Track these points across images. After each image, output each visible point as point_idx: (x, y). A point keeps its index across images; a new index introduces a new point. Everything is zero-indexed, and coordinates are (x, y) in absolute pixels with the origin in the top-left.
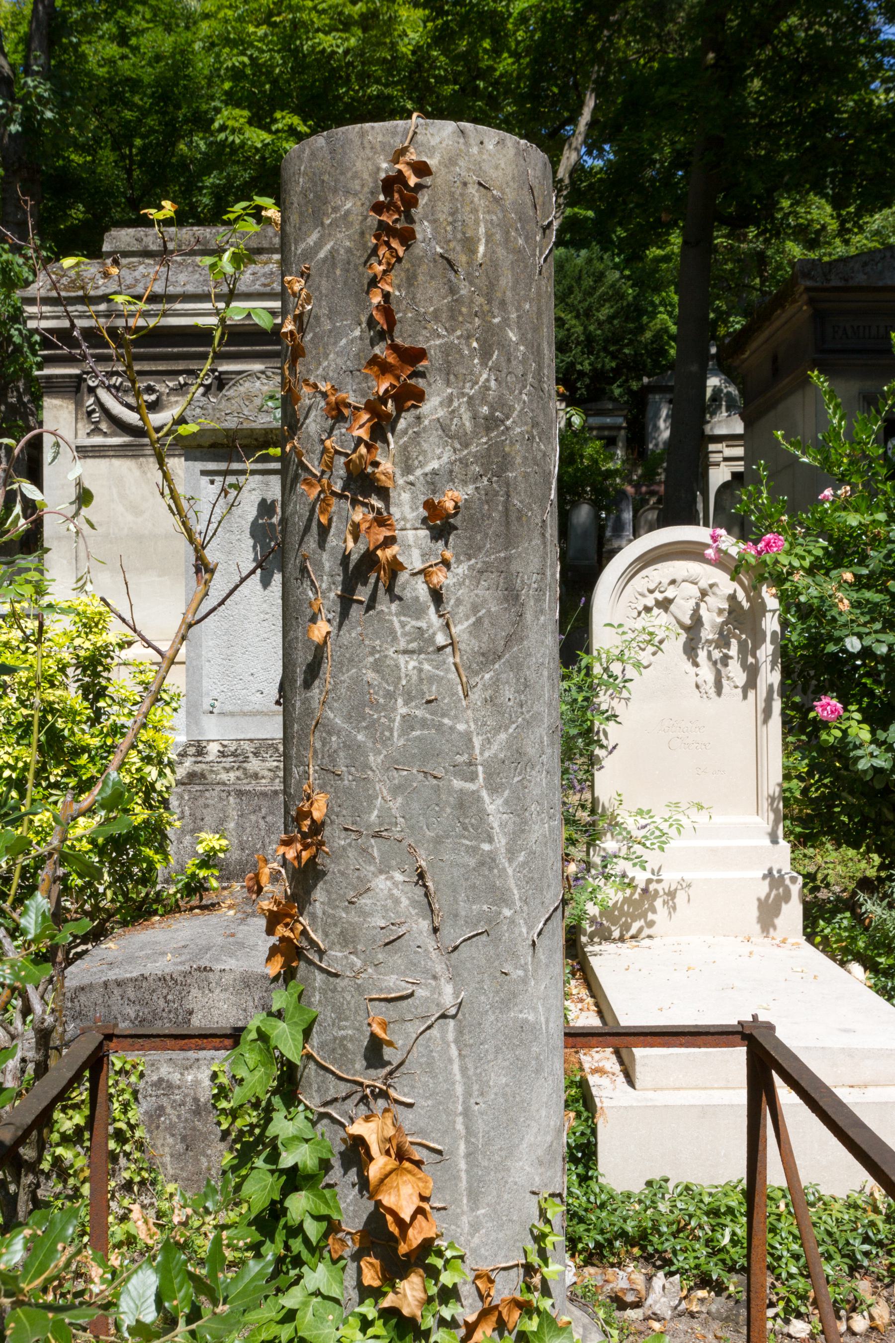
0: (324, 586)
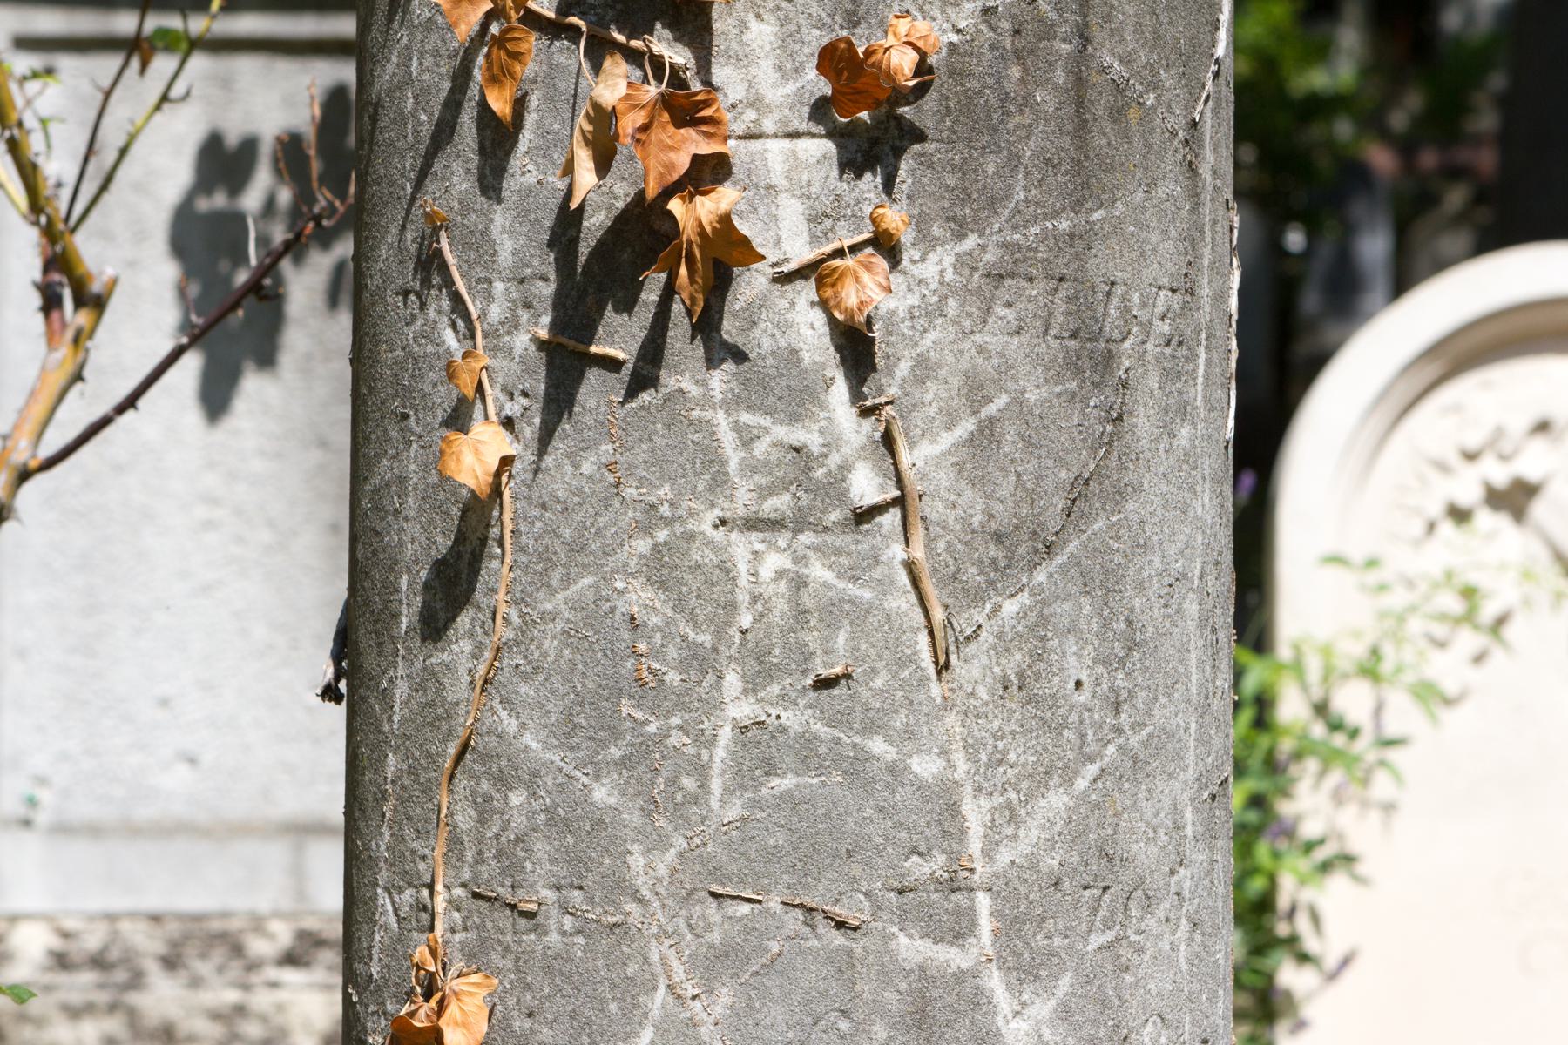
0: (496, 313)
